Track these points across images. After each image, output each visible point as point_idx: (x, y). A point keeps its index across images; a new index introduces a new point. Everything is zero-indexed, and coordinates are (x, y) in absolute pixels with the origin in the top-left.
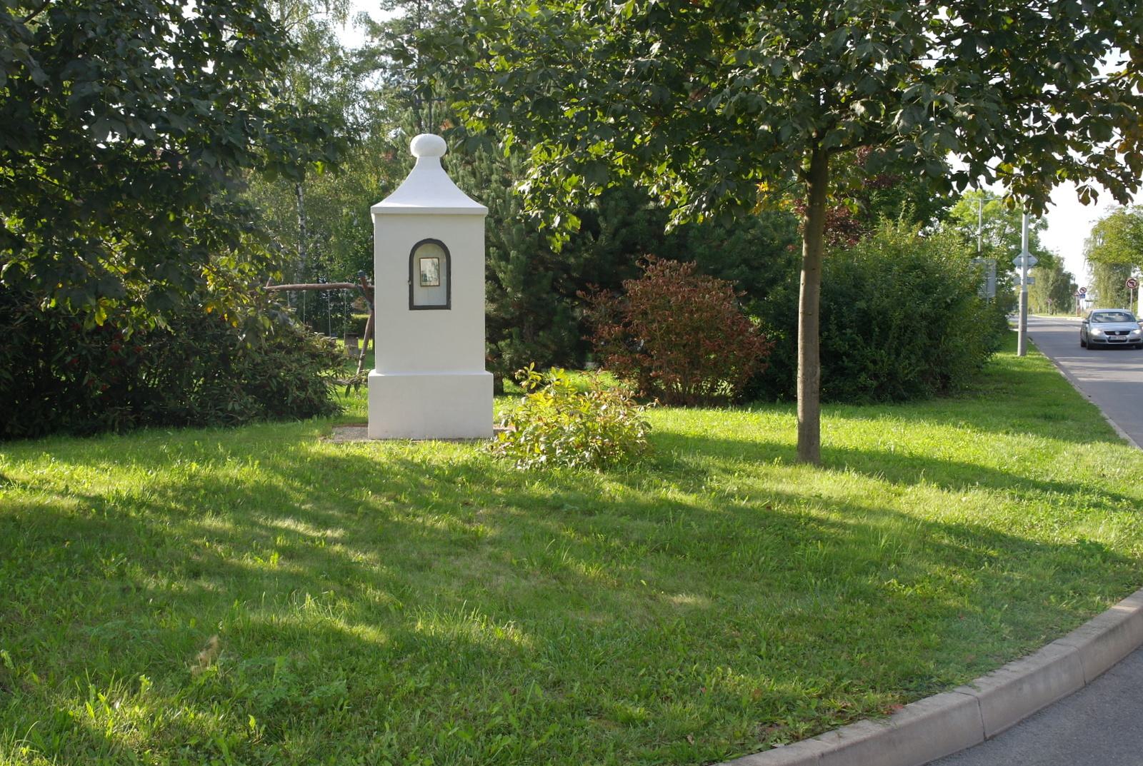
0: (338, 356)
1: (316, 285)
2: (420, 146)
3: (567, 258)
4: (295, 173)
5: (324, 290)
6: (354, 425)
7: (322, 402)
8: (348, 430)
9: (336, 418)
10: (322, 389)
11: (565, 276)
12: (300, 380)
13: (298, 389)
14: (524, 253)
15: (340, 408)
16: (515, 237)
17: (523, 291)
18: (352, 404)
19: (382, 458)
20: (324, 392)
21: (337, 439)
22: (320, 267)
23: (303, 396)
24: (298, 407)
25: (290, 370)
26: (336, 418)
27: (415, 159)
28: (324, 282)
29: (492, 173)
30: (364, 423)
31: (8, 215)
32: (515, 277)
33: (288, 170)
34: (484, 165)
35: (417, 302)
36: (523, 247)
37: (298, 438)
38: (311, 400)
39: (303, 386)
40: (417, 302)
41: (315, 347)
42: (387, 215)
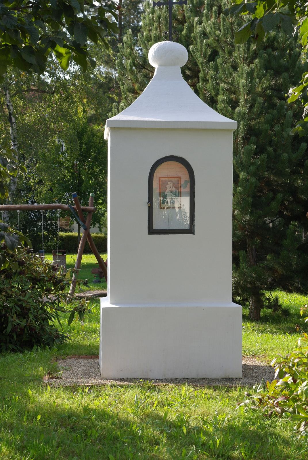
0: (61, 281)
1: (26, 205)
2: (158, 55)
3: (295, 181)
4: (33, 60)
5: (32, 210)
6: (79, 356)
7: (43, 329)
8: (73, 363)
9: (60, 348)
10: (44, 316)
11: (291, 198)
12: (21, 306)
13: (18, 317)
14: (254, 175)
15: (63, 337)
16: (244, 159)
17: (251, 213)
18: (75, 332)
19: (128, 413)
20: (47, 317)
21: (69, 381)
22: (29, 189)
23: (23, 323)
24: (19, 335)
25: (10, 296)
26: (60, 348)
27: (153, 68)
28: (33, 203)
29: (217, 94)
30: (92, 353)
31: (99, 201)
32: (243, 199)
33: (25, 56)
34: (209, 85)
35: (156, 227)
36: (252, 168)
37: (23, 380)
38: (32, 329)
39: (23, 314)
40: (156, 227)
41: (36, 271)
42: (146, 129)
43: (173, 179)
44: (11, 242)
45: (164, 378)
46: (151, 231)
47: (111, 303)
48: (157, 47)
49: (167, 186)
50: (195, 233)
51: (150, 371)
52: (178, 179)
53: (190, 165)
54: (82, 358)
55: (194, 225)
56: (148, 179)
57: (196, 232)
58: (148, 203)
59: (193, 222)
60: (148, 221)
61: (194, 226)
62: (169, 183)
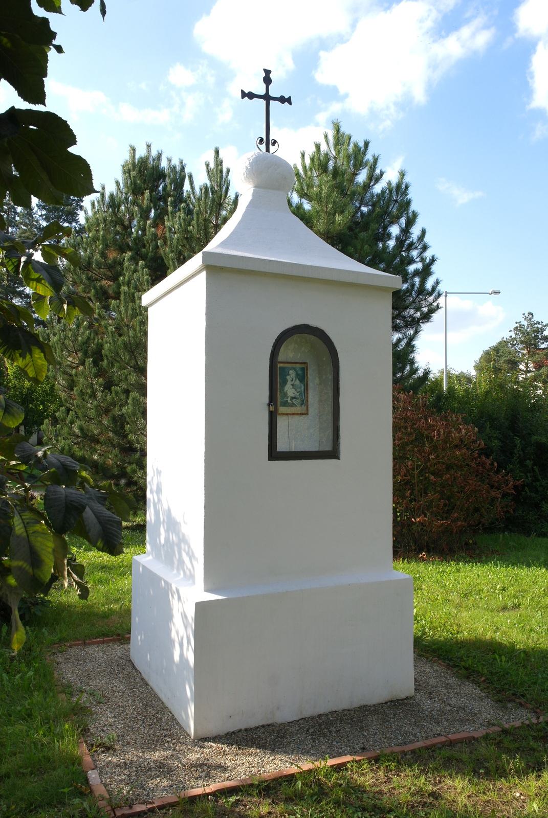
35: (281, 447)
40: (281, 447)
42: (157, 300)
43: (298, 365)
44: (100, 523)
45: (300, 717)
46: (274, 454)
47: (207, 590)
48: (254, 156)
49: (288, 377)
50: (341, 458)
51: (278, 708)
52: (303, 366)
53: (332, 343)
54: (89, 644)
55: (339, 443)
56: (269, 363)
57: (342, 456)
58: (269, 405)
59: (338, 439)
60: (269, 436)
61: (339, 445)
62: (291, 372)
